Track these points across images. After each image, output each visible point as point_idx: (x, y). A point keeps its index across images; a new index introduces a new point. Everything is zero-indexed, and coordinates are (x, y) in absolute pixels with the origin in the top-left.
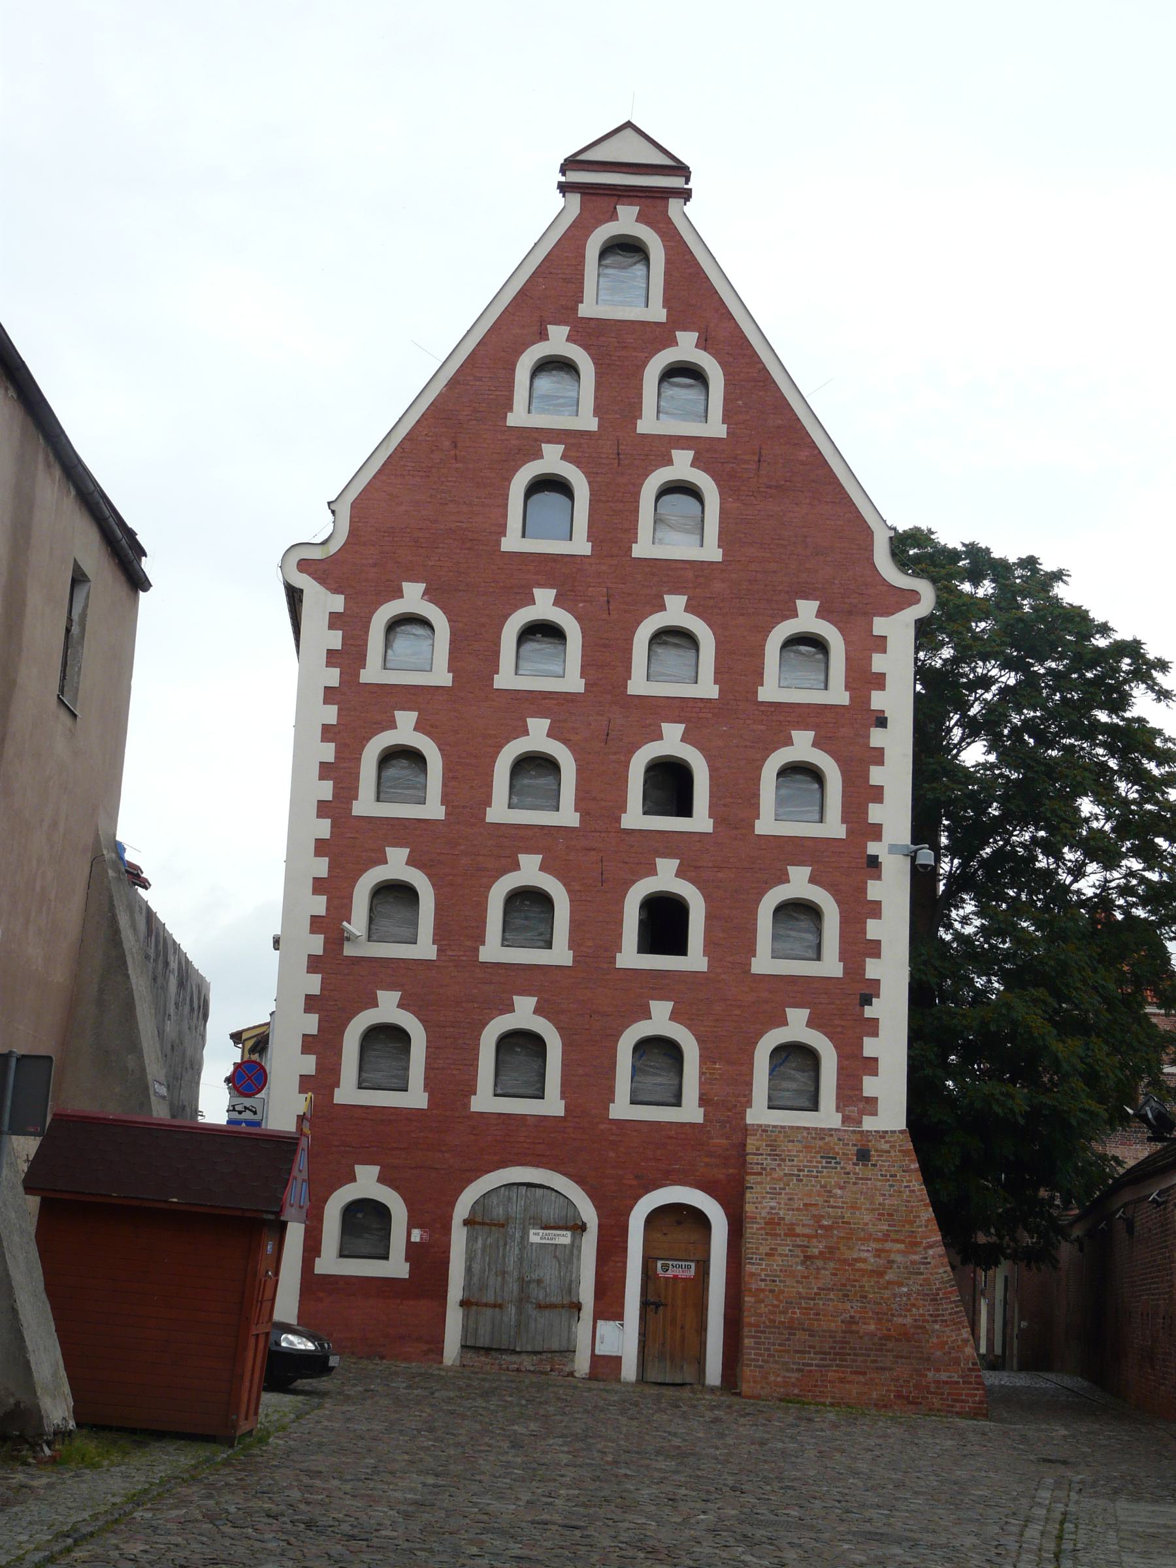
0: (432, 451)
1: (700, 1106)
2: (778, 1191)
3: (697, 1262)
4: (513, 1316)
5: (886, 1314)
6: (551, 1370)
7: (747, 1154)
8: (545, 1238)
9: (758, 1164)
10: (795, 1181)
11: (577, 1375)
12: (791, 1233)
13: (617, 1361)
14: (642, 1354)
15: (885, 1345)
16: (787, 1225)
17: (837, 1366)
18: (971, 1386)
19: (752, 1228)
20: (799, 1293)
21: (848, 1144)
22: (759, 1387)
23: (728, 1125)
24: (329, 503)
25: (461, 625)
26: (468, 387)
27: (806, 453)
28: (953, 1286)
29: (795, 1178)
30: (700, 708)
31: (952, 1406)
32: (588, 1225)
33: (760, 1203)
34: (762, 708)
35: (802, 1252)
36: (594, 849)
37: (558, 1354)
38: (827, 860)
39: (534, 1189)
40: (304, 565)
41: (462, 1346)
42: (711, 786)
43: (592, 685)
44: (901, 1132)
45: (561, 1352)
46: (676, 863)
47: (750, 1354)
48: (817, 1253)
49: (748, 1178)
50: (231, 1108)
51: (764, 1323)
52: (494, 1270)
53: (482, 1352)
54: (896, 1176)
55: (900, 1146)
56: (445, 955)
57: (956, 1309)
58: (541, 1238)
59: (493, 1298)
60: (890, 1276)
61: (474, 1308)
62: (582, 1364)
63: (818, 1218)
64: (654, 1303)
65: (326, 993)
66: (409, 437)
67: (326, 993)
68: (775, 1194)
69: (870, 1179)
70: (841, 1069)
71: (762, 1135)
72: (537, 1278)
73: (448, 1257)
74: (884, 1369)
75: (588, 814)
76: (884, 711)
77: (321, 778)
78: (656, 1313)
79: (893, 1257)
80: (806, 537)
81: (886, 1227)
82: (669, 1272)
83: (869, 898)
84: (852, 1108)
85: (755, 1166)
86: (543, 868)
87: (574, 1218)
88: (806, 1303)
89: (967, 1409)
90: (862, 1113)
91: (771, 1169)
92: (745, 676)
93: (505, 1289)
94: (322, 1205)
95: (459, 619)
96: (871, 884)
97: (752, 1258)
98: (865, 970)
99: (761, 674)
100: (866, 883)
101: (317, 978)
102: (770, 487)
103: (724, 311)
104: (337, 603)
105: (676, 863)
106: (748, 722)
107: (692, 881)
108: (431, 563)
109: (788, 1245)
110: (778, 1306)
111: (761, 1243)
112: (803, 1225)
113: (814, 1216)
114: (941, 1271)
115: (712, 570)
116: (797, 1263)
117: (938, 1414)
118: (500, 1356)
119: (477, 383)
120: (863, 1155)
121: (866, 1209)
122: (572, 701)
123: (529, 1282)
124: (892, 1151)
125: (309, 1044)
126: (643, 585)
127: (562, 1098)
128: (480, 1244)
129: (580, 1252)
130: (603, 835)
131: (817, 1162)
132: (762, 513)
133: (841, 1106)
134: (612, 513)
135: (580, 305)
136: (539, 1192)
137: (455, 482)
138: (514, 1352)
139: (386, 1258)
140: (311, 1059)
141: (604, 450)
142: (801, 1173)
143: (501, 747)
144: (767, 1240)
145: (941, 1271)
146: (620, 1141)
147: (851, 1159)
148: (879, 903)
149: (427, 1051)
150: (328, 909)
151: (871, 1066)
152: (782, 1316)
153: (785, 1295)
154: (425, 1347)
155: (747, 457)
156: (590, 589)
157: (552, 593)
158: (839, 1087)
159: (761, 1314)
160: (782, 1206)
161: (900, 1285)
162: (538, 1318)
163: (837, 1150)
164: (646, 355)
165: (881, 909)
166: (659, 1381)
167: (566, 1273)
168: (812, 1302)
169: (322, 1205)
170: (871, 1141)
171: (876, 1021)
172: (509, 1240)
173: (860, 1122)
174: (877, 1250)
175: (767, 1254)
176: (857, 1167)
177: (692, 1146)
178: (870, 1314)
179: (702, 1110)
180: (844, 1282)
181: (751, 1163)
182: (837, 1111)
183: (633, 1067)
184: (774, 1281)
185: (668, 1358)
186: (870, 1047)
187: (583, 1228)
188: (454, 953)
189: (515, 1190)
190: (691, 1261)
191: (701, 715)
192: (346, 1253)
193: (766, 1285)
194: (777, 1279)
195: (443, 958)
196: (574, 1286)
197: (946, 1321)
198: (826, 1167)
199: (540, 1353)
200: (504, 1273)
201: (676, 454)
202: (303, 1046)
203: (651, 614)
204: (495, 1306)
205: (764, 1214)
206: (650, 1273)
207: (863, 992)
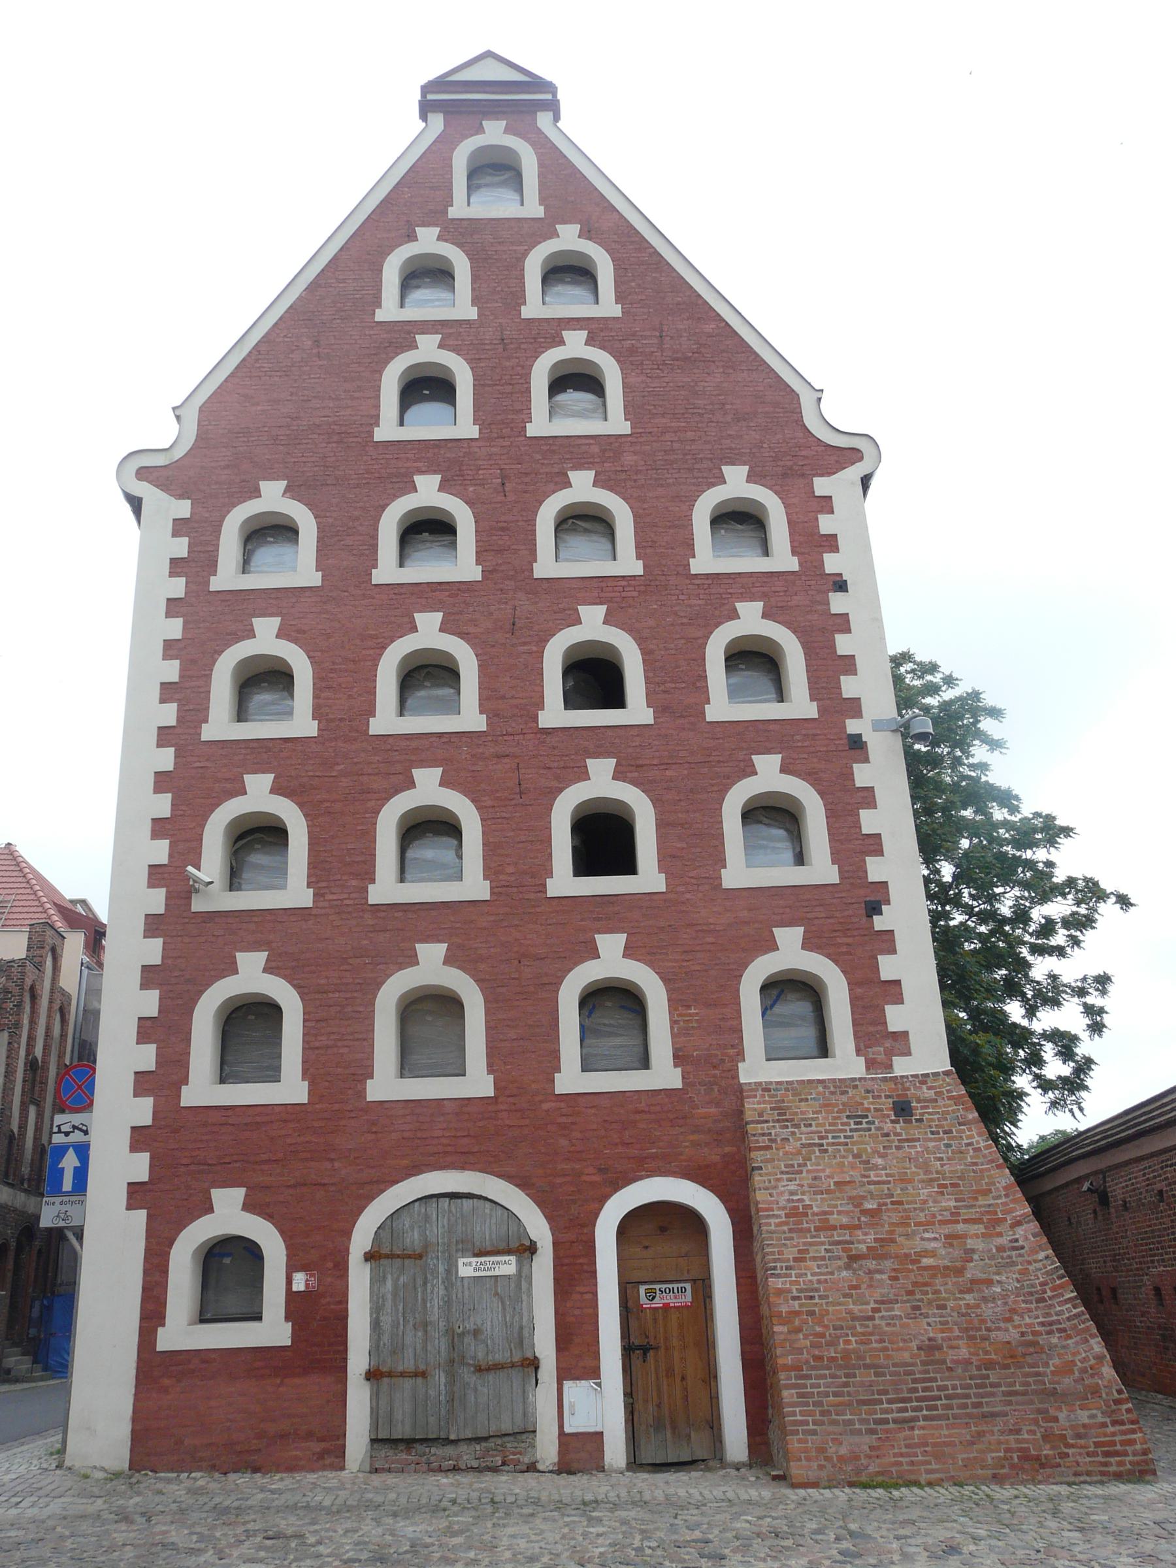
0: (292, 351)
1: (675, 1066)
2: (796, 1168)
3: (694, 1281)
4: (442, 1387)
5: (980, 1329)
6: (504, 1464)
7: (747, 1123)
8: (480, 1269)
9: (763, 1135)
10: (818, 1153)
11: (540, 1467)
12: (826, 1227)
13: (596, 1438)
14: (630, 1424)
15: (987, 1377)
16: (817, 1214)
17: (926, 1418)
18: (1123, 1428)
20: (849, 1312)
21: (879, 1097)
22: (815, 1465)
23: (716, 1088)
24: (174, 409)
25: (330, 520)
26: (331, 289)
27: (714, 326)
28: (1063, 1277)
29: (816, 1149)
31: (1106, 1464)
32: (539, 1245)
33: (775, 1187)
35: (844, 1250)
36: (507, 756)
37: (511, 1438)
38: (800, 744)
40: (144, 474)
41: (374, 1441)
43: (491, 572)
44: (946, 1073)
45: (515, 1434)
46: (612, 762)
47: (794, 1414)
48: (865, 1250)
49: (753, 1154)
51: (807, 1362)
52: (411, 1323)
53: (402, 1447)
54: (950, 1132)
55: (948, 1091)
56: (325, 900)
57: (1075, 1311)
58: (475, 1270)
59: (412, 1362)
60: (973, 1271)
61: (386, 1380)
62: (547, 1449)
63: (857, 1201)
64: (640, 1347)
65: (169, 961)
67: (169, 961)
68: (793, 1172)
69: (918, 1140)
70: (854, 1000)
71: (763, 1096)
72: (473, 1327)
73: (347, 1310)
74: (993, 1415)
75: (497, 715)
76: (841, 574)
77: (163, 701)
78: (644, 1361)
79: (970, 1244)
80: (724, 404)
81: (953, 1203)
82: (657, 1300)
83: (858, 784)
85: (761, 1139)
86: (444, 783)
87: (519, 1238)
88: (861, 1325)
89: (1129, 1466)
90: (890, 1053)
91: (783, 1140)
92: (672, 548)
93: (429, 1348)
94: (167, 1249)
95: (328, 514)
97: (775, 1268)
98: (866, 872)
99: (691, 547)
100: (852, 768)
104: (183, 509)
105: (612, 762)
107: (635, 783)
109: (823, 1243)
110: (823, 1335)
111: (785, 1245)
112: (839, 1213)
113: (850, 1198)
114: (1042, 1255)
115: (621, 443)
116: (839, 1268)
117: (1088, 1479)
118: (427, 1450)
119: (341, 285)
120: (903, 1109)
121: (922, 1181)
122: (468, 590)
123: (463, 1334)
124: (939, 1099)
125: (147, 1030)
126: (542, 464)
127: (490, 1072)
128: (389, 1284)
129: (530, 1284)
130: (517, 738)
131: (843, 1124)
132: (671, 384)
133: (863, 1048)
134: (500, 396)
135: (450, 208)
136: (467, 1204)
137: (319, 378)
138: (448, 1442)
139: (258, 1318)
140: (150, 1050)
142: (824, 1142)
143: (384, 648)
144: (792, 1238)
145: (1042, 1255)
146: (573, 1123)
148: (870, 790)
149: (304, 1026)
150: (171, 856)
151: (893, 991)
152: (832, 1349)
153: (830, 1316)
154: (317, 1447)
156: (480, 472)
157: (437, 479)
158: (855, 1023)
159: (801, 1349)
160: (806, 1188)
161: (989, 1282)
162: (479, 1388)
163: (866, 1106)
164: (526, 248)
165: (874, 796)
166: (658, 1462)
167: (513, 1317)
168: (870, 1323)
169: (167, 1249)
170: (909, 1089)
173: (889, 1067)
174: (947, 1237)
175: (795, 1260)
176: (897, 1126)
177: (671, 1121)
178: (957, 1333)
179: (679, 1070)
180: (910, 1288)
181: (754, 1135)
182: (858, 1055)
183: (582, 1026)
184: (812, 1298)
185: (668, 1426)
186: (888, 968)
187: (531, 1249)
188: (335, 897)
189: (434, 1205)
190: (685, 1281)
191: (624, 594)
192: (209, 1316)
193: (801, 1305)
194: (816, 1294)
195: (321, 904)
196: (526, 1333)
197: (1064, 1330)
198: (856, 1130)
199: (486, 1439)
200: (425, 1325)
201: (567, 335)
202: (138, 1033)
204: (416, 1375)
205: (782, 1203)
206: (630, 1304)
207: (868, 899)
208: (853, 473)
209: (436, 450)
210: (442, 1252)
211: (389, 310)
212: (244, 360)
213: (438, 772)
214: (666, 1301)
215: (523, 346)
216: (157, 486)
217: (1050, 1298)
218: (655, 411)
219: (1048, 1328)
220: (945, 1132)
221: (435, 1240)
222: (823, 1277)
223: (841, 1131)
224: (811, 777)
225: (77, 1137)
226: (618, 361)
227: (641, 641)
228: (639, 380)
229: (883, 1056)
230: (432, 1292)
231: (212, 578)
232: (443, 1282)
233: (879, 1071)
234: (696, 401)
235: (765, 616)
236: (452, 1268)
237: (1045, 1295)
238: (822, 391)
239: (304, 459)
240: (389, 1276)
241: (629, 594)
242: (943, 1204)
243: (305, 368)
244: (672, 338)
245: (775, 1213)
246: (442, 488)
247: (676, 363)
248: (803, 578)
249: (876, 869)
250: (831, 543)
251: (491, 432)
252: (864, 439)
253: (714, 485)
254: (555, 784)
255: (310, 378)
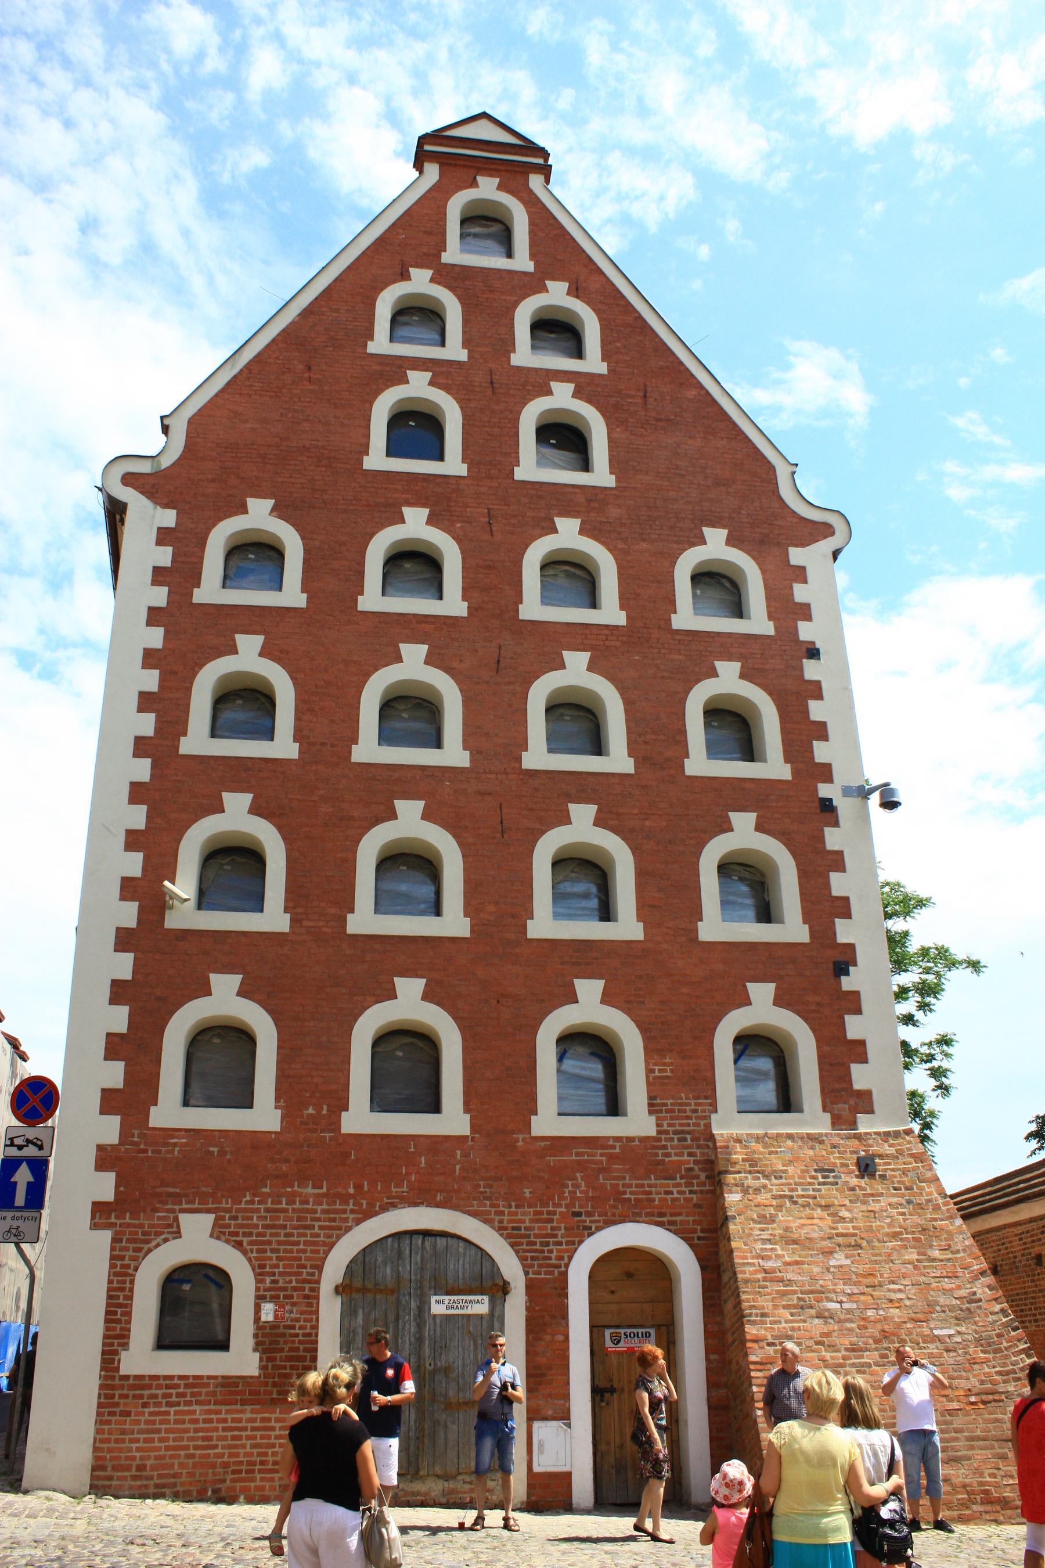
0: (284, 373)
3: (658, 1327)
4: (412, 1423)
15: (951, 1423)
19: (744, 1272)
24: (162, 418)
25: (317, 543)
27: (693, 393)
30: (607, 636)
32: (512, 1285)
34: (679, 637)
36: (490, 794)
39: (433, 1238)
40: (129, 479)
42: (627, 721)
43: (476, 609)
50: (8, 1142)
54: (911, 1189)
56: (301, 927)
58: (447, 1308)
66: (258, 359)
75: (480, 752)
77: (140, 710)
81: (915, 1257)
82: (621, 1344)
84: (840, 1106)
90: (855, 1110)
96: (828, 831)
101: (128, 958)
102: (660, 420)
103: (593, 267)
104: (168, 518)
106: (663, 651)
108: (281, 480)
130: (500, 777)
133: (829, 1105)
136: (441, 1242)
137: (310, 402)
141: (477, 379)
145: (997, 1307)
147: (697, 1177)
150: (144, 869)
155: (633, 393)
162: (449, 1424)
171: (856, 995)
172: (401, 1313)
173: (853, 1125)
188: (312, 924)
189: (408, 1241)
190: (651, 1326)
192: (167, 1342)
203: (541, 536)
208: (826, 546)
209: (425, 484)
210: (414, 1289)
211: (380, 343)
212: (235, 377)
213: (420, 804)
214: (630, 1345)
215: (511, 392)
216: (142, 493)
217: (1006, 1349)
218: (639, 468)
219: (1005, 1377)
220: (907, 1189)
221: (408, 1277)
222: (796, 1325)
223: (810, 1184)
224: (785, 837)
225: (31, 1151)
226: (604, 415)
227: (623, 690)
228: (624, 436)
229: (847, 1112)
230: (403, 1328)
231: (196, 590)
232: (415, 1319)
233: (843, 1127)
234: (679, 463)
235: (743, 676)
236: (423, 1306)
237: (1002, 1346)
238: (797, 465)
239: (292, 480)
240: (360, 1311)
241: (613, 643)
242: (907, 1257)
243: (295, 391)
244: (655, 400)
245: (750, 1261)
246: (430, 521)
247: (659, 423)
248: (779, 643)
249: (844, 932)
250: (805, 612)
251: (479, 471)
252: (836, 515)
253: (694, 545)
254: (538, 826)
255: (300, 401)
